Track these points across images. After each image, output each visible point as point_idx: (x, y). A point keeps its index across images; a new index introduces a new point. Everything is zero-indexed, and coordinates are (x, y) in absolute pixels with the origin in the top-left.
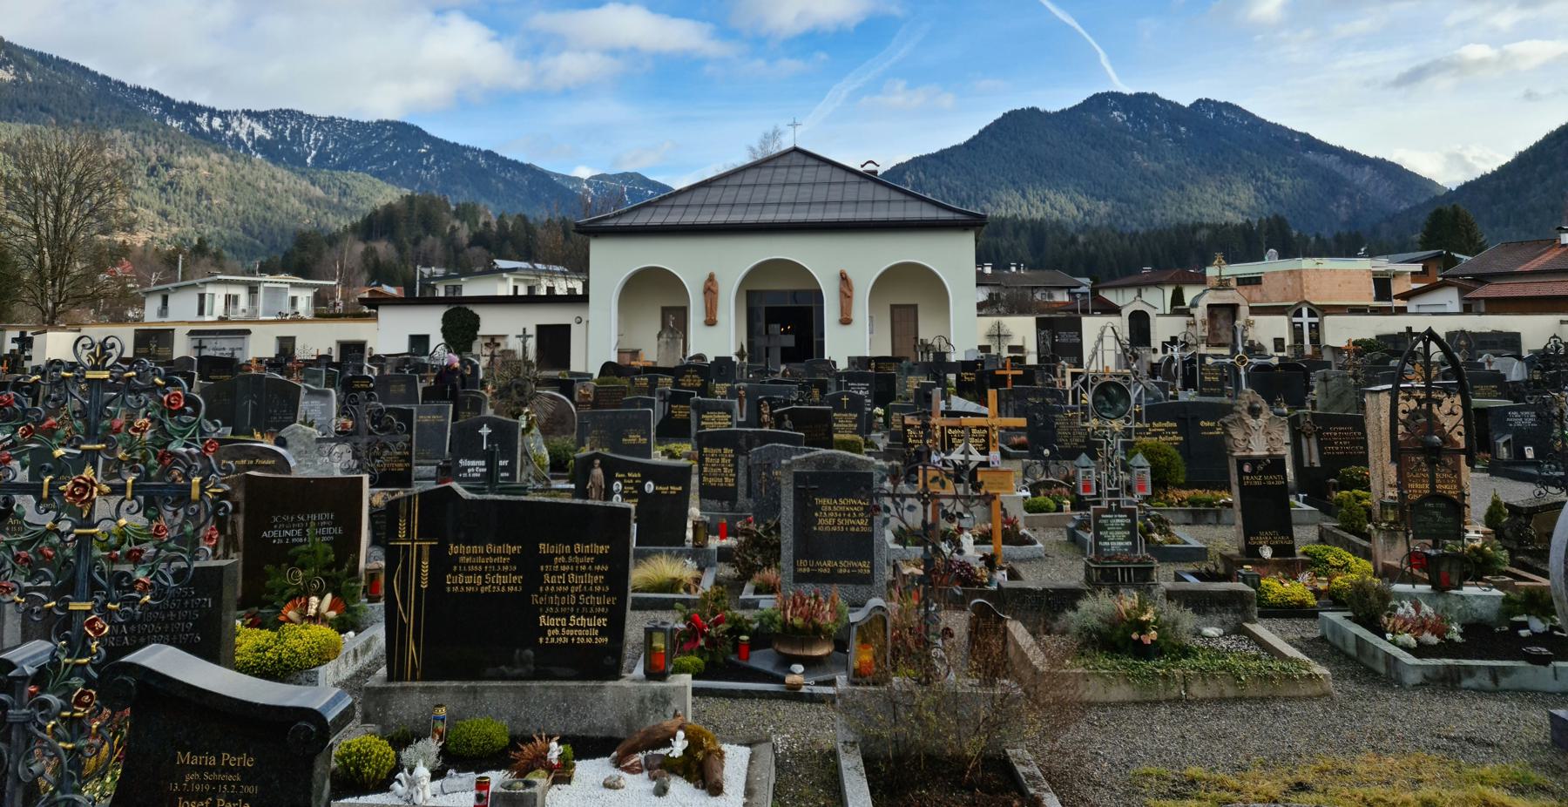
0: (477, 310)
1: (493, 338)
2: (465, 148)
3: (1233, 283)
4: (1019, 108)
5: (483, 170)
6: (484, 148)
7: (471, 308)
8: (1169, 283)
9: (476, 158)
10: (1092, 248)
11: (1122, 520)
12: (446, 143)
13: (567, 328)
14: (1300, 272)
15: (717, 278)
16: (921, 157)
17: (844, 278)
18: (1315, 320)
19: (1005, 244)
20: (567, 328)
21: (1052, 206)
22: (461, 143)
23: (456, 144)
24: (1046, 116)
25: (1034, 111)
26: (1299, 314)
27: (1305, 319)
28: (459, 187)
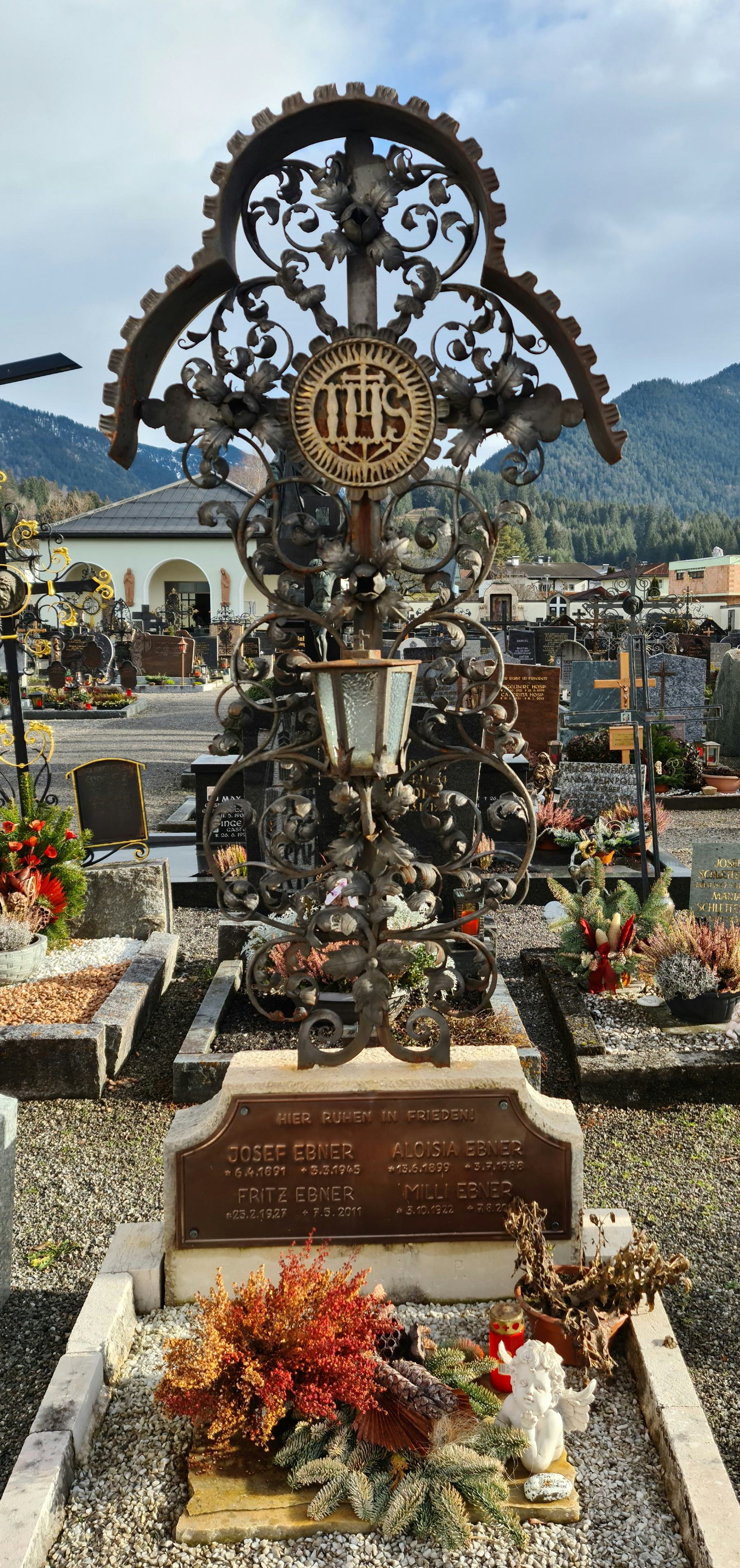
2: (36, 414)
4: (649, 379)
5: (57, 440)
6: (56, 414)
8: (649, 575)
10: (691, 537)
12: (14, 406)
14: (728, 567)
15: (134, 573)
17: (224, 574)
18: (564, 605)
19: (610, 532)
21: (677, 491)
22: (31, 407)
23: (25, 409)
24: (679, 389)
25: (666, 382)
26: (554, 601)
27: (558, 605)
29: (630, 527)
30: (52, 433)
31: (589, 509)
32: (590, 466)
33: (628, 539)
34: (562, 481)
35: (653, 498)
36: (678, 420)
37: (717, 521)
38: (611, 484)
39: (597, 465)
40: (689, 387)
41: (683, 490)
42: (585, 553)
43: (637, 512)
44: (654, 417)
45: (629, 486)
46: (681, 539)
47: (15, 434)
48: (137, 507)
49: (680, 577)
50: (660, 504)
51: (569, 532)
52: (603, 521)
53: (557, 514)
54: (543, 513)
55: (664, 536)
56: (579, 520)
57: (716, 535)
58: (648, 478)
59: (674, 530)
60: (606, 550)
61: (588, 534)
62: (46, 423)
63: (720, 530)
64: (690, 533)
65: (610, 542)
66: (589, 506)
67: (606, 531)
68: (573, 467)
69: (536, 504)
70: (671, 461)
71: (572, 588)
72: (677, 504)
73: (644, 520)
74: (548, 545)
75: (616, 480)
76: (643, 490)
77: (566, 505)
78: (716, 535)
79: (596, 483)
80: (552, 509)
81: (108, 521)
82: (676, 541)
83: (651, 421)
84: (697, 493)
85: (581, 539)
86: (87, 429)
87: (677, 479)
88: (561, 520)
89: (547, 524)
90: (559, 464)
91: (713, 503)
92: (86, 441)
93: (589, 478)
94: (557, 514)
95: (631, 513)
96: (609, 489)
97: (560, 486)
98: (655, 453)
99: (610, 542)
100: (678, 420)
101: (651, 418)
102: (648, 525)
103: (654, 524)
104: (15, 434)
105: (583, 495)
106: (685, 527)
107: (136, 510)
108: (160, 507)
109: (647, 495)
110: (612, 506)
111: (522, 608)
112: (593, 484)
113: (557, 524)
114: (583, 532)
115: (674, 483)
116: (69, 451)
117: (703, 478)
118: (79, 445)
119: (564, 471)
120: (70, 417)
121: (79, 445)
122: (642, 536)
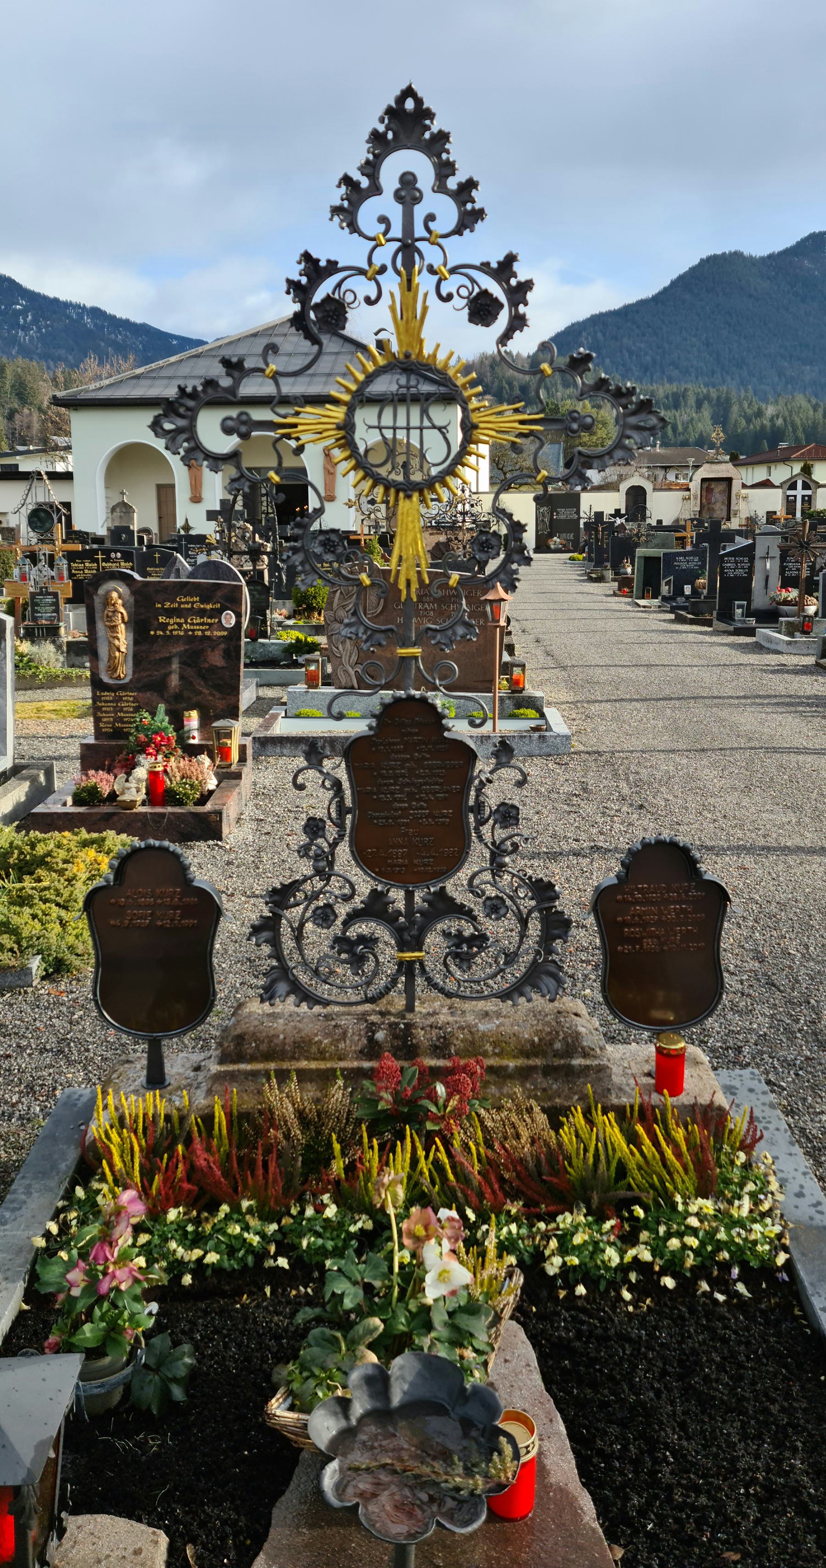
2: (67, 305)
4: (719, 252)
5: (90, 331)
6: (89, 305)
8: (798, 460)
9: (80, 316)
11: (49, 599)
16: (601, 315)
18: (809, 492)
19: (685, 418)
22: (62, 298)
23: (56, 300)
24: (751, 262)
26: (793, 486)
27: (799, 492)
28: (62, 352)
29: (707, 412)
30: (85, 325)
36: (751, 296)
40: (763, 259)
43: (714, 394)
46: (767, 423)
47: (47, 326)
52: (676, 406)
55: (749, 421)
59: (759, 414)
62: (78, 314)
65: (686, 429)
76: (713, 373)
81: (165, 382)
82: (763, 427)
86: (120, 320)
99: (686, 429)
100: (751, 296)
103: (735, 409)
104: (47, 326)
106: (770, 411)
111: (745, 498)
120: (103, 308)
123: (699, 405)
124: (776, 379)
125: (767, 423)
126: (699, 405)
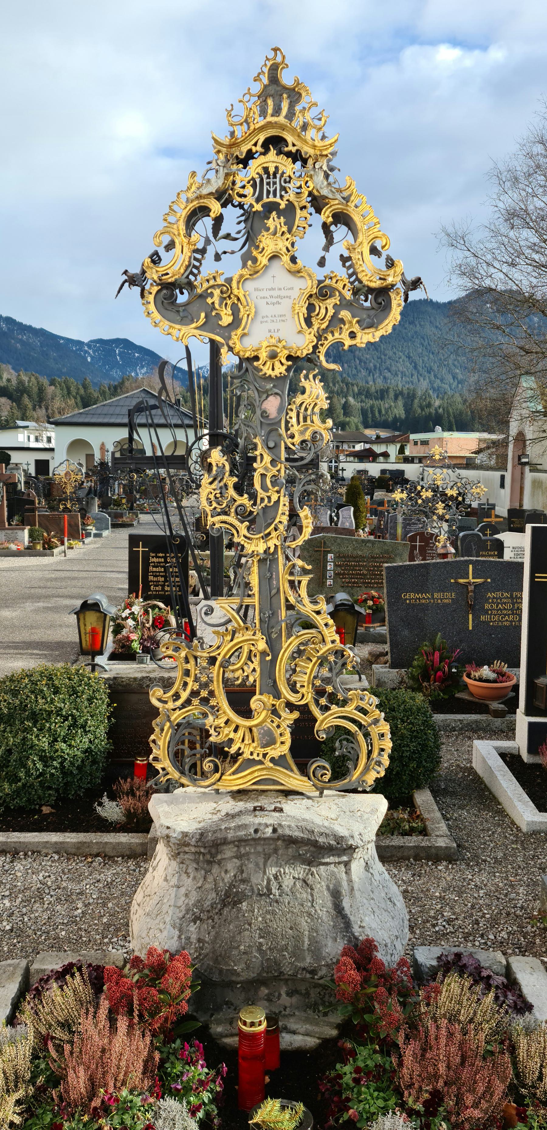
0: (10, 452)
1: (17, 464)
3: (419, 443)
5: (4, 333)
6: (4, 315)
7: (7, 451)
8: (398, 442)
10: (441, 410)
13: (48, 461)
19: (387, 405)
20: (48, 461)
26: (331, 462)
27: (333, 464)
29: (400, 403)
30: (2, 328)
31: (373, 390)
32: (376, 358)
33: (399, 411)
34: (356, 368)
35: (419, 381)
36: (437, 327)
37: (459, 399)
38: (390, 371)
39: (380, 358)
41: (439, 377)
42: (370, 420)
43: (405, 392)
44: (420, 325)
45: (402, 373)
46: (434, 412)
48: (106, 408)
49: (416, 443)
50: (423, 386)
51: (359, 405)
52: (382, 398)
53: (351, 393)
54: (342, 392)
55: (422, 409)
56: (366, 397)
57: (457, 410)
58: (415, 367)
59: (429, 405)
60: (383, 418)
61: (372, 407)
63: (460, 406)
64: (439, 407)
65: (387, 412)
66: (373, 388)
67: (384, 405)
68: (364, 359)
69: (337, 385)
70: (431, 356)
71: (354, 447)
72: (435, 385)
73: (410, 397)
74: (344, 414)
75: (394, 368)
76: (412, 376)
77: (357, 386)
78: (457, 410)
79: (380, 370)
80: (348, 389)
82: (430, 413)
83: (418, 328)
84: (449, 378)
85: (367, 410)
86: (25, 326)
87: (435, 368)
88: (354, 397)
89: (344, 400)
90: (354, 357)
91: (460, 386)
92: (25, 334)
93: (375, 366)
94: (351, 393)
95: (401, 393)
96: (388, 375)
97: (354, 371)
98: (420, 350)
99: (387, 412)
100: (437, 327)
101: (418, 326)
102: (413, 401)
103: (416, 401)
105: (370, 379)
106: (437, 403)
107: (106, 410)
108: (119, 408)
109: (415, 379)
110: (388, 388)
112: (377, 371)
113: (351, 400)
114: (368, 405)
115: (434, 371)
116: (13, 341)
117: (453, 367)
118: (20, 337)
119: (358, 362)
120: (14, 318)
121: (20, 337)
122: (408, 408)
123: (396, 397)
124: (452, 381)
125: (433, 411)
126: (396, 397)
